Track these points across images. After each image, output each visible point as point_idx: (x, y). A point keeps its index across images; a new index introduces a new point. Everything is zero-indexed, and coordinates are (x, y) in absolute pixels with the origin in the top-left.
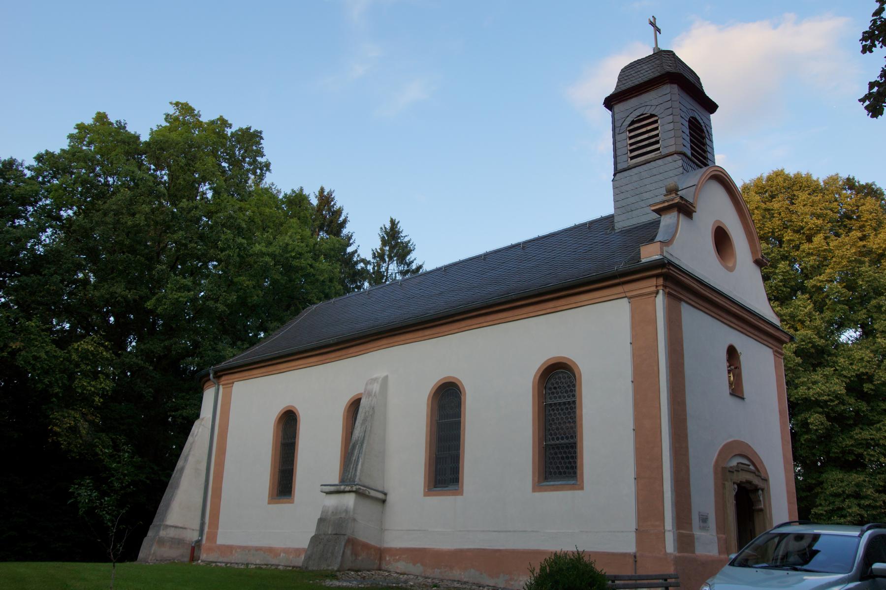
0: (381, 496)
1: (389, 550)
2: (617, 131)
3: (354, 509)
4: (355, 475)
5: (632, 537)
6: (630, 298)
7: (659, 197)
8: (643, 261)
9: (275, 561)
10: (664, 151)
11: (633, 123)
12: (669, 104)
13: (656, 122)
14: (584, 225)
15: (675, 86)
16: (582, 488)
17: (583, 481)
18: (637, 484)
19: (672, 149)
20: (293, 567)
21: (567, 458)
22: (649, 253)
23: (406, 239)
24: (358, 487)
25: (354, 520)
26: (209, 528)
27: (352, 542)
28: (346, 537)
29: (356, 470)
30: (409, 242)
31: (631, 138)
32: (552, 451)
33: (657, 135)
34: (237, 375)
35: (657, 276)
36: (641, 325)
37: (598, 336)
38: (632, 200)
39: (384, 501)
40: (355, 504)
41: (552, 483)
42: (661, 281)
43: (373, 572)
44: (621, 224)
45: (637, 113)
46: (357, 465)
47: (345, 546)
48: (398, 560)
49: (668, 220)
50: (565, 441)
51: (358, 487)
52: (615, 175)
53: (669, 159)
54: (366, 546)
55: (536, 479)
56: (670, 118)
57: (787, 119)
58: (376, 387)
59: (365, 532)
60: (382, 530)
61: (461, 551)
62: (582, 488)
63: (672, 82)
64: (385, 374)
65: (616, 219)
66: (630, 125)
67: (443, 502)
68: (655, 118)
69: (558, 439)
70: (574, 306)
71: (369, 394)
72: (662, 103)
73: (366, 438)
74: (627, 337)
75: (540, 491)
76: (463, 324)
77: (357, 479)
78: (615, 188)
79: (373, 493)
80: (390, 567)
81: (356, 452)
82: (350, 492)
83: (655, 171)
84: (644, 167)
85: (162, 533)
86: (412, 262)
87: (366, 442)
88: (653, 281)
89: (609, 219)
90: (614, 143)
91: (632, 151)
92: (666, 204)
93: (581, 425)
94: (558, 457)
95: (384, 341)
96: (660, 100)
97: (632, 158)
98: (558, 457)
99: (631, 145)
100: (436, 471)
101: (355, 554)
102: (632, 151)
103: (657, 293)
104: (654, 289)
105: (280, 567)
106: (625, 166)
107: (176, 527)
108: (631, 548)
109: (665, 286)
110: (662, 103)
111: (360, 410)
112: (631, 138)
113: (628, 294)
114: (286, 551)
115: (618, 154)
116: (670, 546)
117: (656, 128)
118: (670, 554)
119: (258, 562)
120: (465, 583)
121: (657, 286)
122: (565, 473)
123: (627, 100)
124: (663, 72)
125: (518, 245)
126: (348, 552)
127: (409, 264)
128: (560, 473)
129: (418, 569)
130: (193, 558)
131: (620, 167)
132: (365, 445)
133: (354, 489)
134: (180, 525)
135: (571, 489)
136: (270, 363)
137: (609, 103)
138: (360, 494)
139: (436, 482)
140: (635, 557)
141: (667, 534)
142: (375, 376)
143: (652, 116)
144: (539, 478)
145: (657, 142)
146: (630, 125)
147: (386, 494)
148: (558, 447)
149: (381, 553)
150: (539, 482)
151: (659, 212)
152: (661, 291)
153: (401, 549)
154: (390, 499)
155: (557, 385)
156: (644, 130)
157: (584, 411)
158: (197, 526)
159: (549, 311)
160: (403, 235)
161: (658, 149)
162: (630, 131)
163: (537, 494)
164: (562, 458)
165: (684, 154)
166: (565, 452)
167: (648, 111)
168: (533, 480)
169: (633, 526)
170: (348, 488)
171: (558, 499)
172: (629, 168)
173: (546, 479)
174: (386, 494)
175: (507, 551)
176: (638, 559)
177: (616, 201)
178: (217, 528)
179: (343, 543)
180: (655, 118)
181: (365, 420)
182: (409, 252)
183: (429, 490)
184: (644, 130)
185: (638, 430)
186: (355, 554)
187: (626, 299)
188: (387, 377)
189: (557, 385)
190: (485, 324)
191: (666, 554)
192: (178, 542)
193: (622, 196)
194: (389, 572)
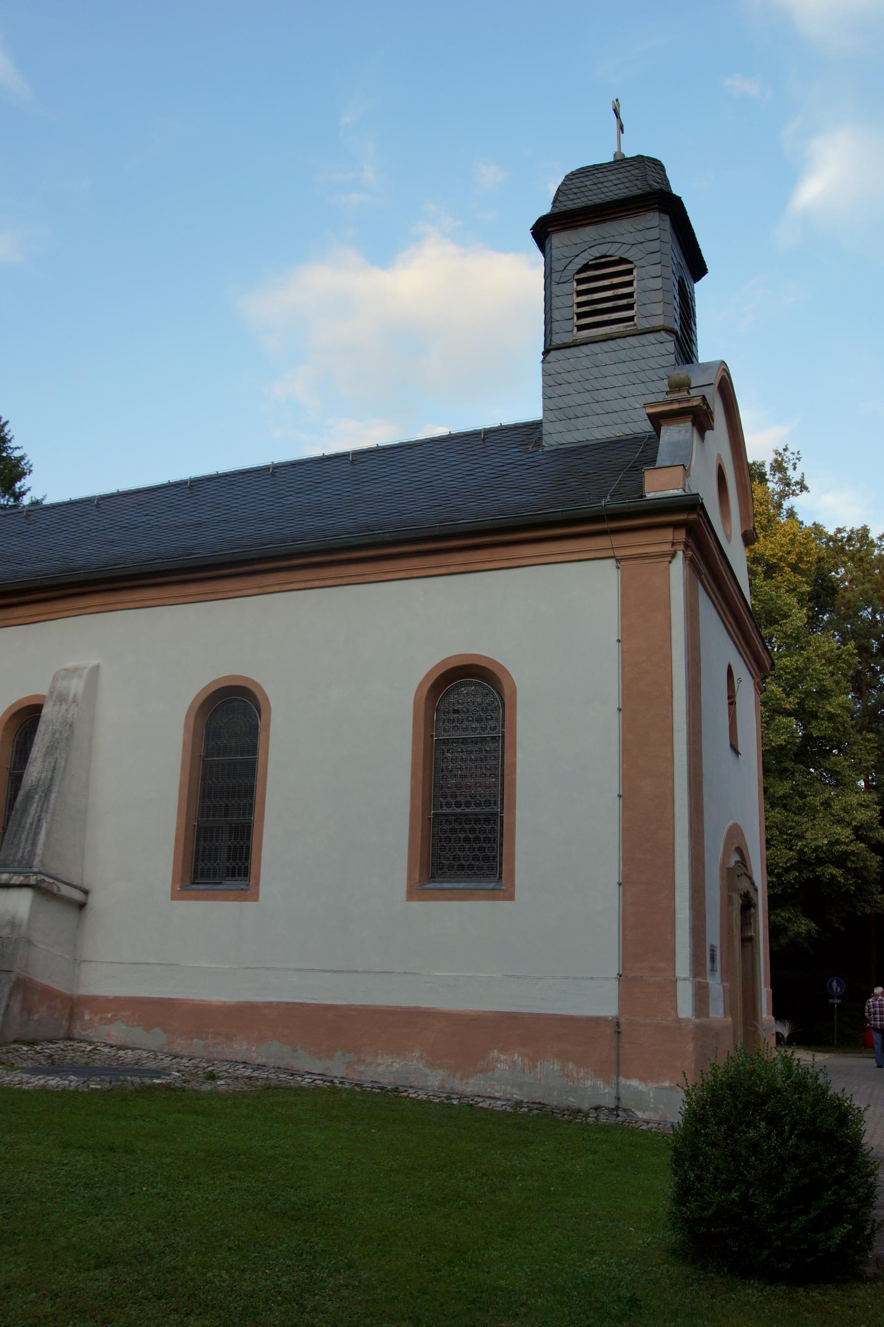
0: (77, 895)
1: (91, 1002)
2: (556, 277)
3: (30, 920)
4: (32, 853)
5: (613, 988)
6: (618, 560)
7: (656, 393)
8: (649, 496)
10: (641, 323)
11: (585, 268)
12: (656, 246)
14: (475, 434)
15: (667, 218)
16: (512, 898)
17: (513, 885)
19: (658, 322)
21: (477, 840)
22: (659, 486)
23: (17, 454)
24: (40, 877)
25: (29, 942)
27: (24, 987)
28: (13, 977)
29: (34, 844)
30: (22, 458)
31: (580, 293)
32: (445, 827)
33: (630, 295)
35: (676, 526)
36: (639, 613)
37: (558, 627)
38: (578, 399)
39: (81, 906)
40: (33, 910)
41: (446, 885)
42: (681, 535)
43: (61, 1045)
44: (553, 439)
45: (596, 252)
46: (37, 834)
47: (11, 994)
48: (111, 1021)
49: (674, 434)
50: (473, 809)
51: (40, 877)
52: (546, 353)
53: (651, 337)
54: (48, 994)
55: (416, 876)
56: (657, 270)
58: (76, 686)
59: (46, 969)
60: (77, 962)
61: (252, 1007)
62: (512, 898)
63: (662, 210)
64: (94, 662)
65: (546, 428)
66: (580, 271)
67: (214, 913)
68: (629, 266)
69: (458, 805)
70: (462, 569)
71: (62, 698)
72: (621, 239)
73: (57, 783)
74: (613, 630)
77: (37, 861)
78: (546, 374)
79: (66, 891)
80: (91, 1034)
81: (34, 808)
82: (21, 886)
83: (623, 355)
84: (603, 345)
86: (24, 493)
87: (55, 789)
88: (668, 534)
89: (534, 427)
90: (548, 299)
91: (580, 316)
92: (676, 406)
93: (514, 781)
94: (463, 834)
96: (640, 237)
97: (580, 328)
98: (463, 834)
99: (580, 305)
100: (197, 852)
101: (28, 1010)
102: (580, 316)
103: (673, 555)
104: (667, 548)
106: (568, 339)
108: (609, 1008)
109: (686, 546)
110: (621, 239)
111: (42, 727)
112: (580, 293)
115: (556, 315)
116: (685, 1008)
117: (630, 284)
118: (687, 1020)
120: (260, 1067)
121: (673, 544)
122: (471, 867)
123: (576, 227)
124: (648, 189)
125: (344, 456)
126: (16, 1007)
127: (18, 496)
128: (461, 867)
129: (156, 1039)
131: (557, 340)
132: (53, 796)
133: (33, 880)
135: (488, 899)
136: (74, 591)
137: (543, 231)
138: (42, 891)
139: (196, 873)
140: (618, 1024)
142: (70, 664)
143: (622, 261)
144: (421, 875)
145: (630, 307)
146: (580, 271)
147: (86, 892)
149: (73, 1006)
150: (421, 882)
151: (657, 420)
152: (680, 554)
153: (117, 999)
154: (96, 901)
155: (465, 711)
156: (606, 282)
157: (520, 756)
160: (13, 444)
161: (631, 319)
162: (580, 282)
163: (417, 905)
164: (467, 840)
165: (675, 333)
166: (472, 830)
167: (616, 251)
168: (410, 879)
169: (613, 967)
170: (16, 880)
171: (460, 916)
172: (575, 345)
173: (432, 878)
174: (86, 892)
175: (349, 1008)
176: (623, 1028)
177: (546, 397)
179: (7, 989)
180: (629, 266)
181: (52, 749)
182: (21, 475)
183: (183, 887)
184: (606, 282)
185: (629, 797)
186: (28, 1010)
187: (611, 563)
188: (97, 667)
189: (465, 711)
190: (317, 583)
191: (678, 1021)
193: (559, 390)
194: (91, 1043)
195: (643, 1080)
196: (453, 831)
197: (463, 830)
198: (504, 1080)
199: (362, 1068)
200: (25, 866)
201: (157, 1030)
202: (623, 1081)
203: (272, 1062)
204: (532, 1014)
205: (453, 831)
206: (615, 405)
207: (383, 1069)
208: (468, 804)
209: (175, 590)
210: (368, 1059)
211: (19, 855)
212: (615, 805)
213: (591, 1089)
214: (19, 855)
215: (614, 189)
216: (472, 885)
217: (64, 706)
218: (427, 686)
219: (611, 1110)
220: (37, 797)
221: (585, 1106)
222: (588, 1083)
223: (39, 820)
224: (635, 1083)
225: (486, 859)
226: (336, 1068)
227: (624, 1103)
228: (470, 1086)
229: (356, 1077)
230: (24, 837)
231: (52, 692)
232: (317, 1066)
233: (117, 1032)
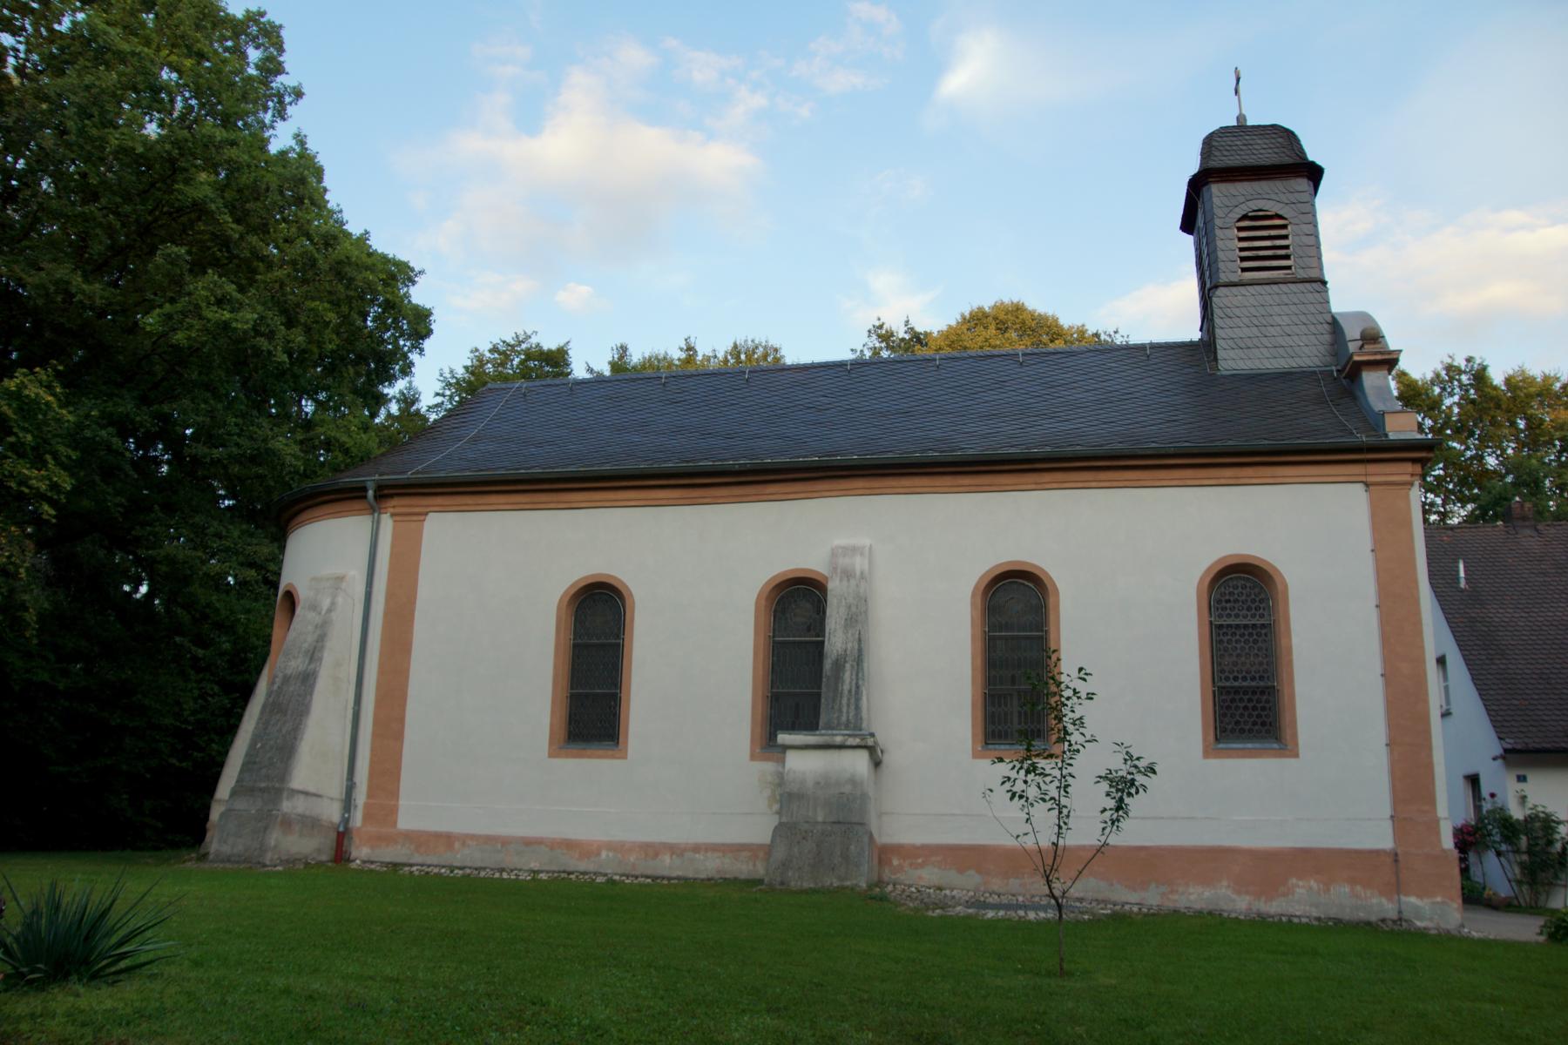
1: (898, 849)
5: (1387, 827)
6: (1367, 485)
9: (583, 866)
11: (1244, 217)
13: (1284, 227)
16: (1296, 755)
18: (1391, 753)
20: (654, 878)
21: (1255, 708)
26: (370, 795)
34: (439, 500)
35: (1414, 461)
36: (1386, 528)
45: (1254, 205)
48: (921, 866)
57: (1457, 270)
58: (859, 563)
62: (1296, 755)
66: (1240, 220)
67: (591, 768)
72: (1251, 188)
75: (1217, 756)
76: (1047, 477)
80: (901, 877)
81: (847, 676)
85: (286, 806)
88: (1409, 467)
94: (1248, 701)
95: (860, 483)
97: (1244, 270)
98: (1248, 701)
99: (1241, 249)
102: (1243, 259)
103: (1412, 484)
104: (1407, 478)
105: (543, 876)
106: (1234, 278)
107: (306, 794)
108: (1387, 843)
110: (1251, 188)
112: (1241, 239)
113: (1370, 479)
114: (618, 847)
119: (534, 865)
122: (1250, 731)
130: (341, 855)
134: (312, 789)
141: (1442, 823)
143: (1281, 217)
145: (1287, 257)
148: (1237, 691)
155: (1242, 604)
157: (1295, 640)
158: (336, 789)
159: (1223, 481)
161: (1289, 268)
162: (1240, 229)
163: (1215, 763)
169: (1387, 810)
178: (395, 794)
184: (1273, 233)
187: (1360, 488)
189: (1242, 604)
191: (1444, 851)
192: (311, 824)
195: (1420, 896)
196: (1233, 701)
197: (1241, 700)
198: (1302, 900)
199: (1176, 897)
200: (855, 725)
201: (972, 872)
202: (1403, 898)
203: (1090, 895)
204: (1323, 850)
205: (1233, 701)
206: (1280, 341)
207: (1195, 896)
208: (1244, 679)
209: (948, 480)
210: (1181, 889)
211: (844, 719)
212: (1379, 682)
213: (1379, 905)
214: (844, 719)
215: (1265, 155)
216: (1257, 746)
217: (853, 582)
218: (1208, 579)
219: (1394, 922)
220: (848, 666)
221: (1373, 918)
222: (1374, 901)
223: (858, 687)
224: (1413, 899)
225: (1263, 724)
226: (1153, 898)
227: (1406, 915)
228: (1274, 907)
229: (1171, 905)
230: (844, 701)
231: (835, 569)
232: (1133, 897)
233: (928, 876)
